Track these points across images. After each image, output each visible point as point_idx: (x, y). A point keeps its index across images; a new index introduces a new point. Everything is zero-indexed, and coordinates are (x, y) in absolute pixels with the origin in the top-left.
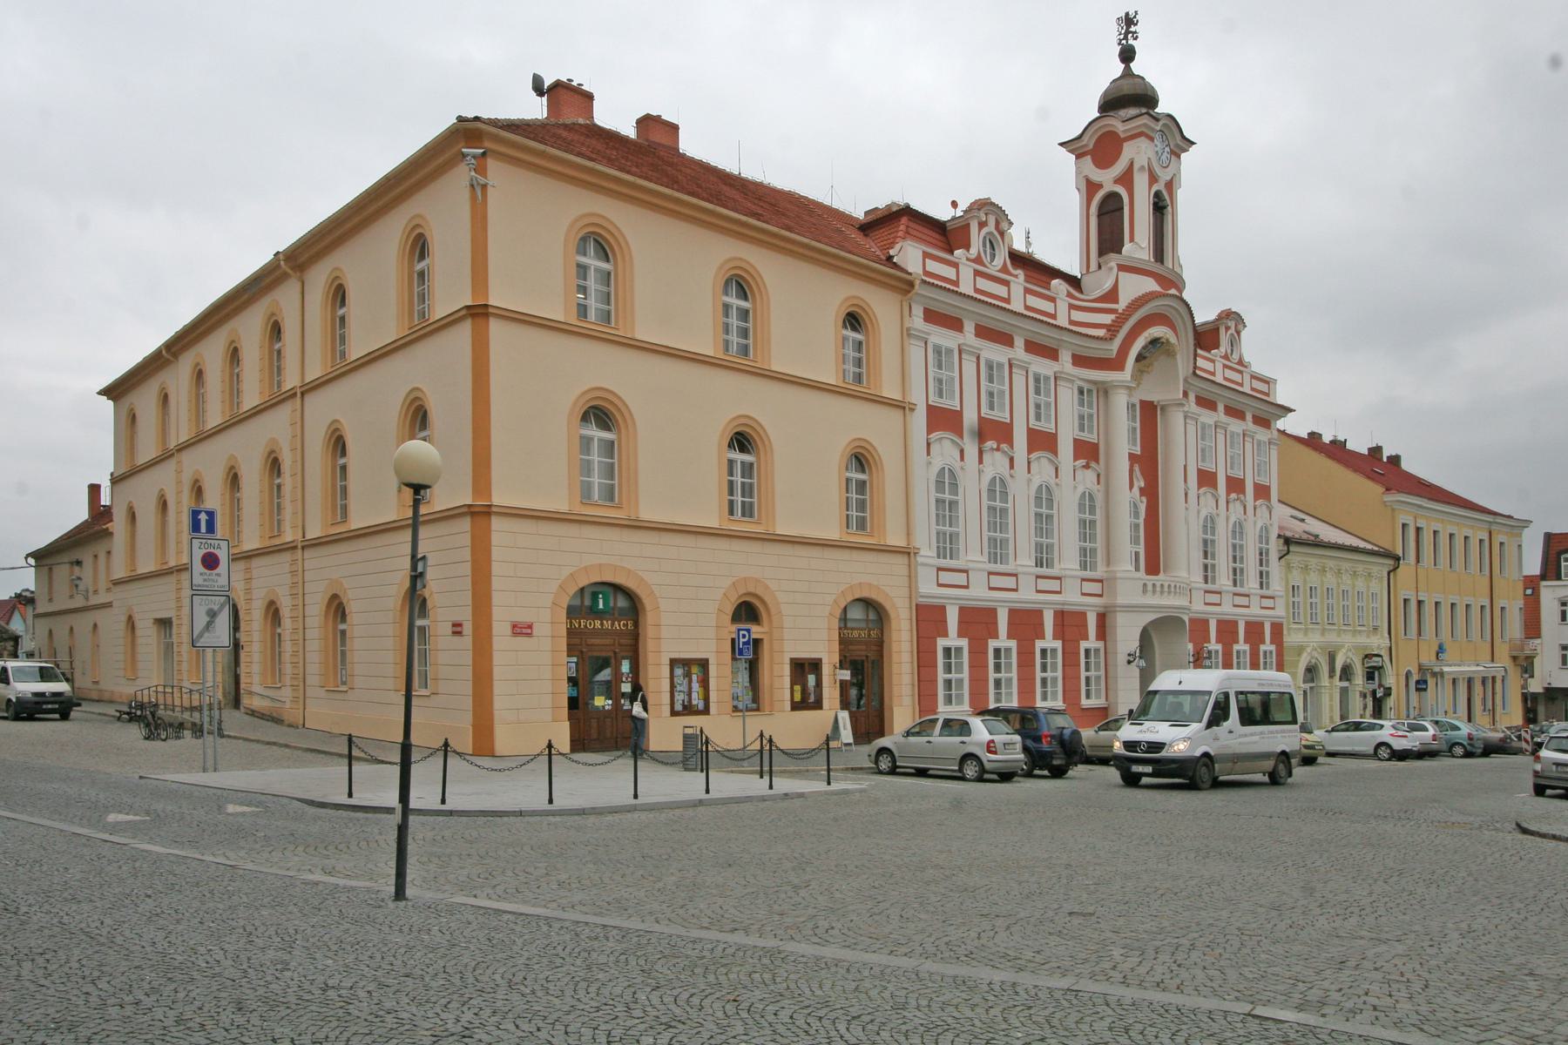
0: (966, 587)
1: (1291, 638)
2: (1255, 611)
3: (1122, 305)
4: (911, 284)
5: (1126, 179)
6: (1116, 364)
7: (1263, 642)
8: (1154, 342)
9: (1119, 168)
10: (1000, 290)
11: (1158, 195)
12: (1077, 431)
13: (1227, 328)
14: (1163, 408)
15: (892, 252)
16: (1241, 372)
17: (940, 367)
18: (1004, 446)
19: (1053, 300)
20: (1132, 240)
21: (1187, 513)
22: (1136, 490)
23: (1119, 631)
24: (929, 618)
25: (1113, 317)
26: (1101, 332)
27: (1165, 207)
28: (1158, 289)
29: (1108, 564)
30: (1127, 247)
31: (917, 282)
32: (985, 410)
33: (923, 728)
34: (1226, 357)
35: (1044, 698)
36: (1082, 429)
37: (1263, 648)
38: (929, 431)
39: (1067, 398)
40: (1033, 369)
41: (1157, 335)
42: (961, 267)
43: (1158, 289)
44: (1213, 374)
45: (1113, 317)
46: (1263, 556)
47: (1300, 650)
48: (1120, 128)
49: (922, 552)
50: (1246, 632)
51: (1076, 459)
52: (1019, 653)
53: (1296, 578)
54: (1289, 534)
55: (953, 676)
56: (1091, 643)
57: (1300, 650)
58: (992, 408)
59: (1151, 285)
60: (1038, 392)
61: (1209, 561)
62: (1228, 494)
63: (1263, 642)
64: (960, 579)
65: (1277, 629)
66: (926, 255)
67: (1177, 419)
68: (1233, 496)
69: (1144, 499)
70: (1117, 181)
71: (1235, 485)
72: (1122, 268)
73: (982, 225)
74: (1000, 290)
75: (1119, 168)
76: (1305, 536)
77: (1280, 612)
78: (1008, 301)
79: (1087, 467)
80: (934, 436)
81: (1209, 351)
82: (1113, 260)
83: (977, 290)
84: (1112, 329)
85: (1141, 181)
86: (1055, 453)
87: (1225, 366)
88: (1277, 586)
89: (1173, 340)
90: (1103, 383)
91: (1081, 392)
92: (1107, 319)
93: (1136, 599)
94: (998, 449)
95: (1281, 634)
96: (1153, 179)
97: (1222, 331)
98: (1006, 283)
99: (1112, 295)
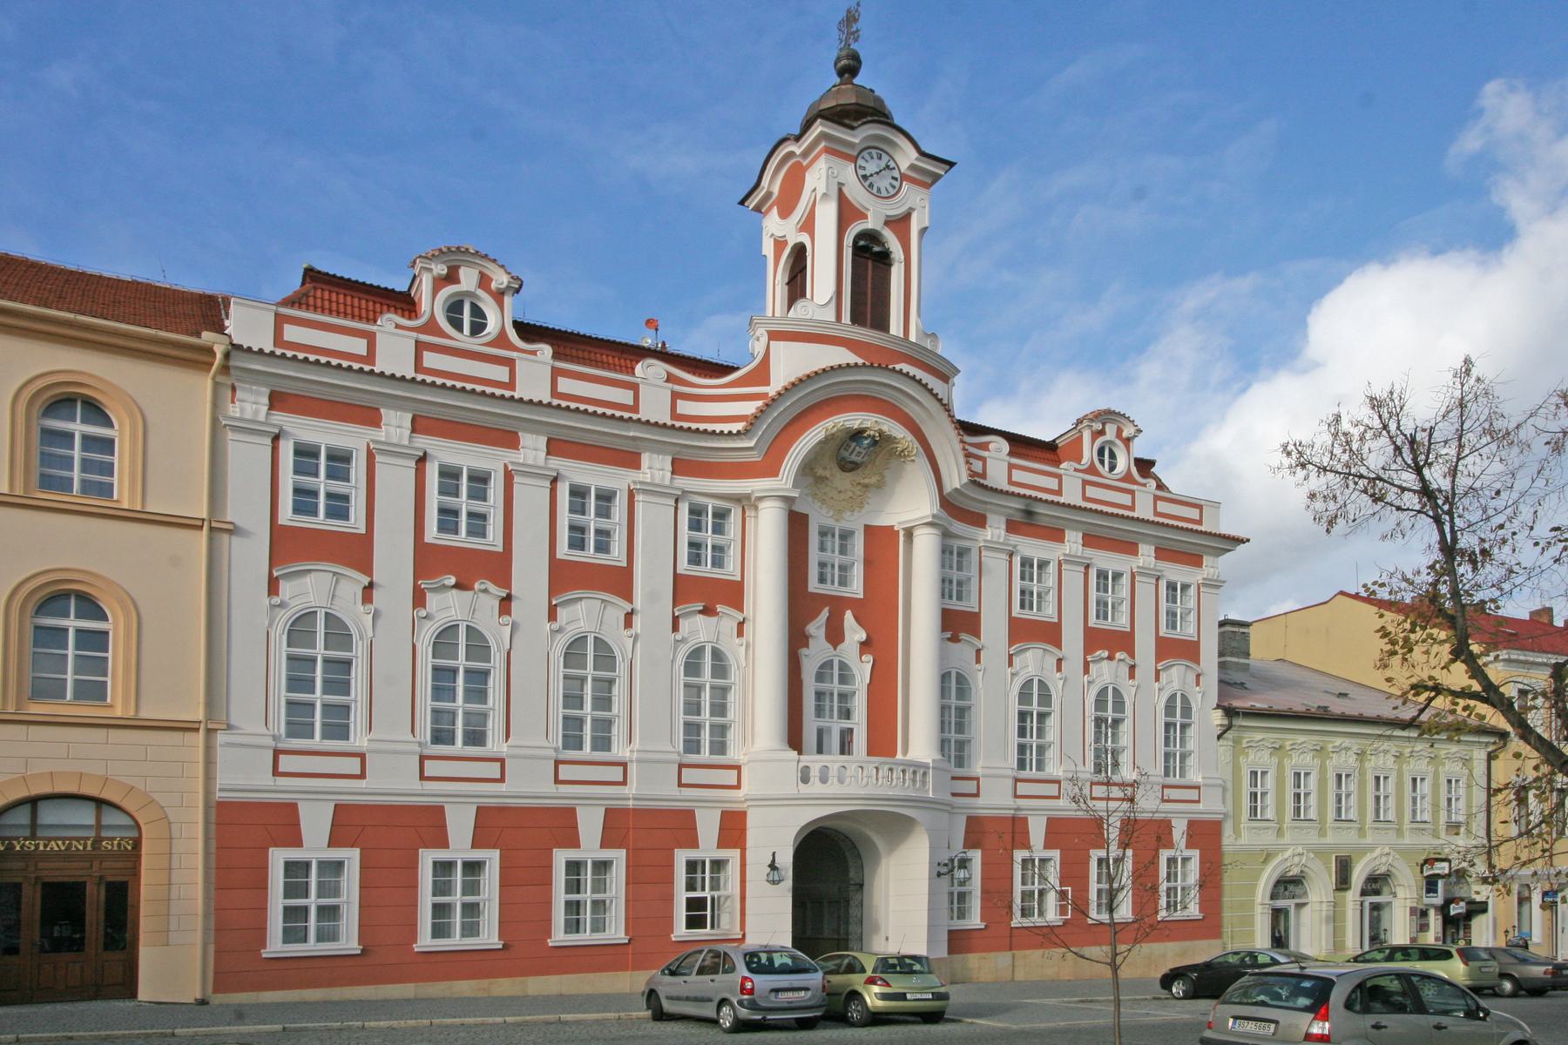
10: (1125, 499)
12: (286, 515)
14: (909, 534)
25: (760, 403)
45: (760, 403)
65: (1205, 834)
74: (1125, 499)
92: (750, 408)
99: (761, 374)
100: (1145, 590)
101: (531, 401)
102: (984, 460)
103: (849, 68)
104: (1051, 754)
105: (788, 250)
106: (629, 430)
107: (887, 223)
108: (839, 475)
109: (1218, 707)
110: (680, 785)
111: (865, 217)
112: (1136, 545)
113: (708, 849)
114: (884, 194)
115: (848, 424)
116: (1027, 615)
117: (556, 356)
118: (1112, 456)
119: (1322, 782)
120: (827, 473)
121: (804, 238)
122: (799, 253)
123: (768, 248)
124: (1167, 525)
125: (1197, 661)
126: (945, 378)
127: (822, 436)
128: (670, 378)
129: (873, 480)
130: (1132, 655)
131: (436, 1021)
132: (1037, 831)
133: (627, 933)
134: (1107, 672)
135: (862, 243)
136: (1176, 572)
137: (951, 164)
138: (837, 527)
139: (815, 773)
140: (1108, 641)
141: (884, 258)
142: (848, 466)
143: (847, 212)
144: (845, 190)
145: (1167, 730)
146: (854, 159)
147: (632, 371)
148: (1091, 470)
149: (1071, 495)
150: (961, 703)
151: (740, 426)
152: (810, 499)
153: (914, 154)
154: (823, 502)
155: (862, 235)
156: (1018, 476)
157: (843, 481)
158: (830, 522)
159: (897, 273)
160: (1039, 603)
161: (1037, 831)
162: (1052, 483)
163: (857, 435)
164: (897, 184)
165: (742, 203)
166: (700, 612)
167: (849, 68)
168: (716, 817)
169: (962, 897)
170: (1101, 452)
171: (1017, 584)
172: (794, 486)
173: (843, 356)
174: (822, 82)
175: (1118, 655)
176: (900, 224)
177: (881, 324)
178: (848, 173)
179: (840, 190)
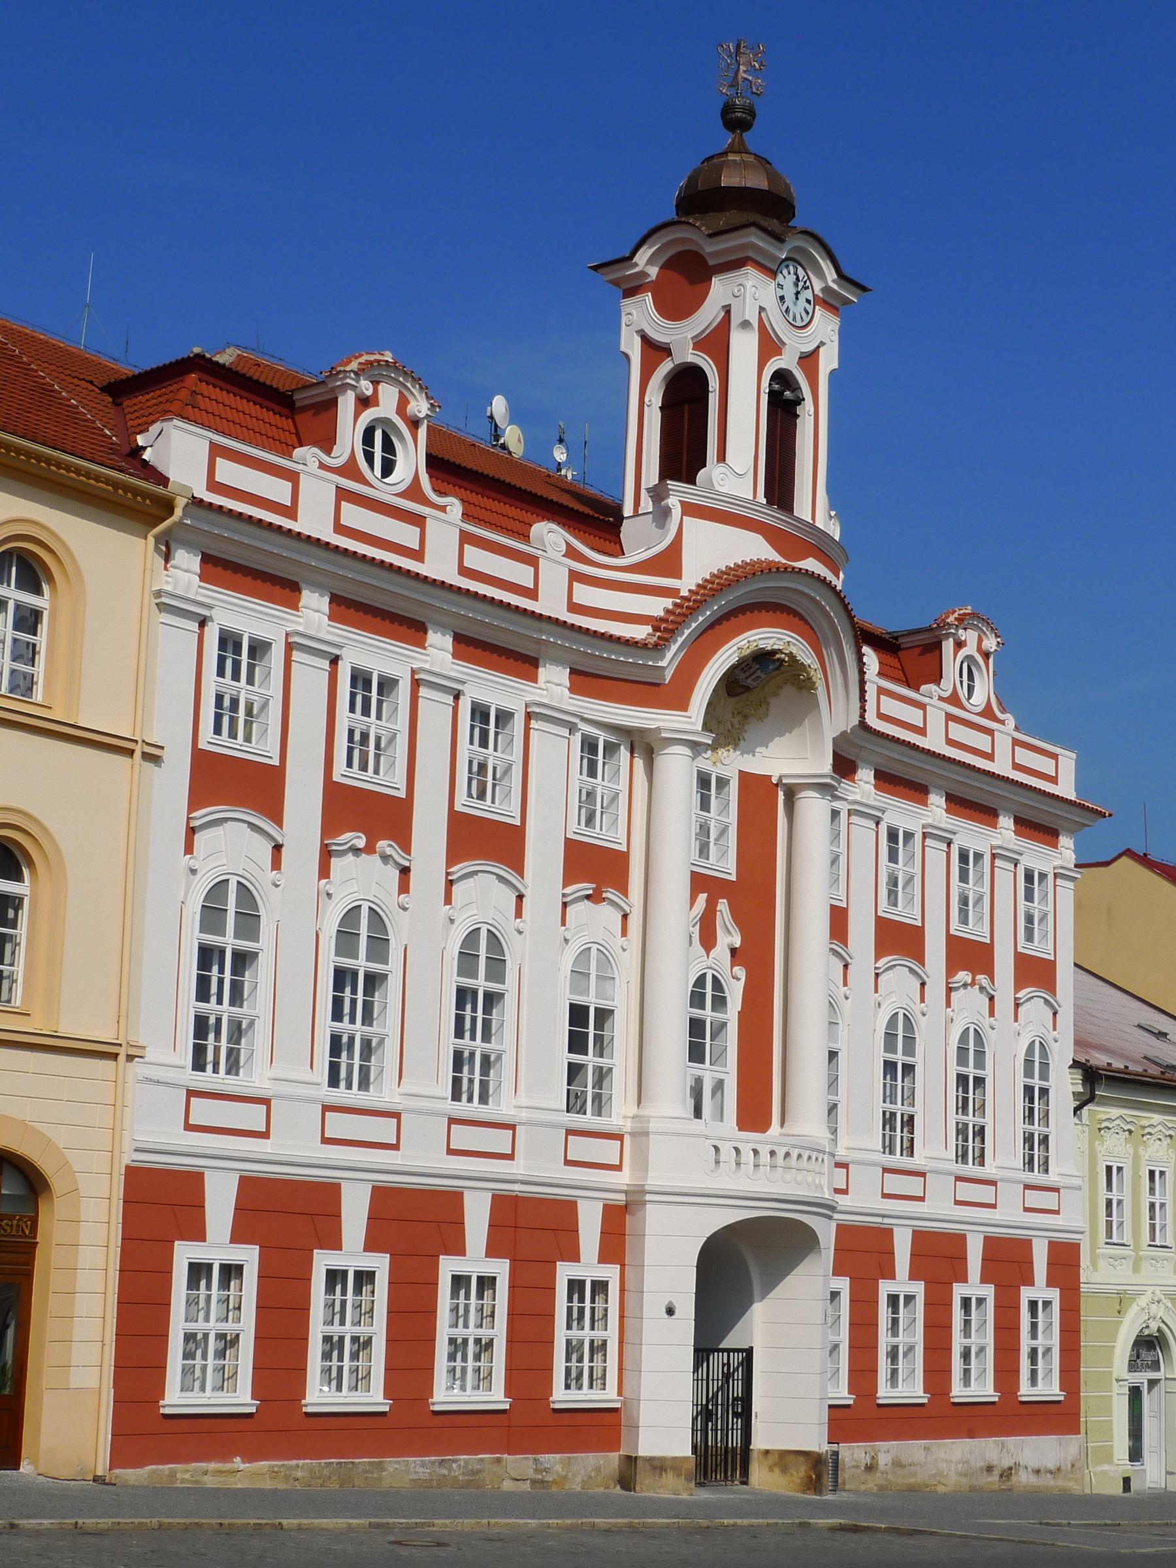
0: (265, 1135)
1: (1095, 1275)
2: (1009, 1215)
3: (687, 583)
4: (167, 506)
5: (716, 342)
6: (674, 696)
7: (889, 1273)
8: (762, 658)
9: (707, 316)
10: (407, 535)
11: (782, 377)
12: (573, 826)
13: (959, 645)
14: (791, 793)
15: (141, 440)
16: (990, 732)
17: (484, 743)
18: (982, 979)
19: (532, 561)
20: (722, 457)
21: (833, 1004)
22: (721, 951)
23: (650, 1244)
24: (160, 1203)
25: (668, 603)
26: (640, 632)
27: (799, 401)
28: (773, 556)
29: (782, 1124)
30: (712, 472)
31: (180, 503)
32: (956, 928)
33: (857, 1418)
34: (954, 700)
35: (573, 1380)
36: (704, 850)
37: (1026, 1294)
38: (1017, 988)
39: (554, 757)
40: (1026, 862)
41: (768, 645)
42: (303, 480)
43: (773, 556)
44: (922, 731)
45: (668, 603)
46: (1035, 1097)
47: (1122, 1300)
48: (709, 248)
49: (151, 1055)
50: (1051, 1264)
51: (567, 882)
52: (512, 1287)
53: (1115, 1149)
54: (1100, 1059)
55: (587, 1334)
56: (589, 1265)
57: (1122, 1300)
58: (964, 920)
59: (755, 548)
60: (964, 878)
61: (590, 1059)
62: (951, 971)
63: (889, 1273)
64: (499, 1141)
65: (1065, 1261)
66: (216, 451)
67: (813, 807)
68: (963, 976)
69: (740, 972)
70: (701, 344)
71: (969, 956)
72: (690, 510)
73: (364, 402)
74: (407, 535)
75: (707, 316)
76: (1154, 1071)
77: (1074, 1218)
78: (532, 594)
79: (595, 898)
80: (458, 869)
81: (914, 685)
82: (678, 494)
83: (464, 571)
84: (666, 628)
85: (743, 347)
86: (921, 960)
87: (950, 717)
88: (1067, 1160)
89: (805, 654)
90: (642, 732)
91: (590, 746)
92: (657, 606)
93: (691, 1171)
94: (370, 849)
95: (1076, 1266)
96: (769, 346)
97: (948, 646)
98: (418, 521)
99: (669, 561)
100: (435, 712)
104: (257, 1043)
106: (541, 631)
109: (1076, 1064)
110: (189, 1127)
112: (996, 816)
113: (589, 1265)
116: (223, 745)
117: (466, 516)
118: (388, 447)
119: (1136, 1179)
124: (399, 570)
125: (277, 817)
127: (734, 660)
128: (571, 553)
130: (406, 847)
131: (493, 1521)
132: (220, 1203)
133: (507, 1394)
134: (363, 877)
136: (490, 687)
139: (805, 1157)
140: (367, 816)
144: (822, 350)
145: (339, 985)
147: (525, 537)
148: (349, 470)
149: (314, 521)
150: (245, 945)
153: (831, 274)
156: (227, 472)
160: (248, 724)
161: (220, 1203)
162: (279, 490)
164: (810, 308)
166: (588, 897)
168: (598, 1208)
169: (835, 1347)
170: (368, 438)
171: (465, 750)
172: (706, 727)
175: (382, 845)
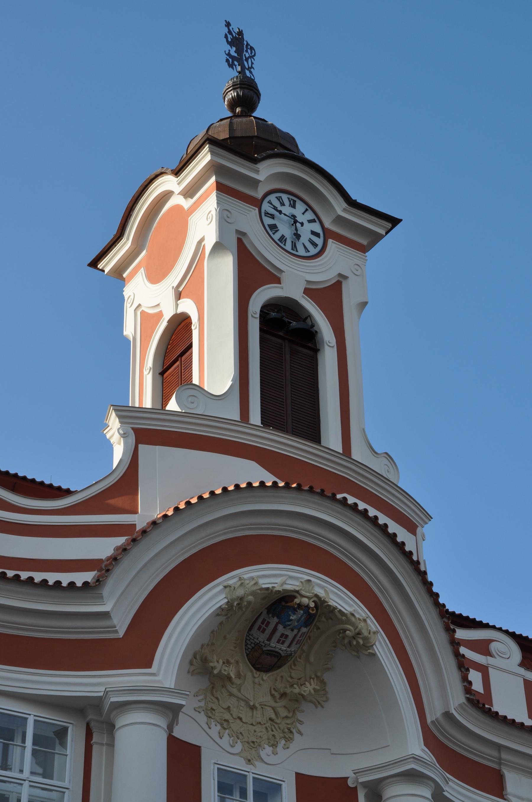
25: (120, 541)
92: (103, 548)
101: (437, 595)
102: (484, 670)
103: (247, 97)
105: (163, 325)
107: (308, 292)
108: (250, 675)
111: (278, 281)
114: (301, 252)
115: (265, 583)
120: (232, 672)
121: (187, 306)
122: (180, 326)
123: (130, 328)
126: (412, 528)
127: (221, 601)
129: (308, 688)
135: (273, 315)
137: (394, 222)
138: (254, 771)
141: (309, 338)
142: (264, 661)
143: (251, 273)
146: (257, 203)
151: (89, 576)
152: (202, 718)
154: (224, 724)
155: (268, 308)
157: (258, 688)
158: (238, 764)
159: (328, 360)
163: (280, 603)
165: (94, 264)
167: (247, 97)
173: (255, 473)
174: (215, 109)
176: (330, 296)
177: (312, 431)
178: (249, 220)
179: (240, 242)
